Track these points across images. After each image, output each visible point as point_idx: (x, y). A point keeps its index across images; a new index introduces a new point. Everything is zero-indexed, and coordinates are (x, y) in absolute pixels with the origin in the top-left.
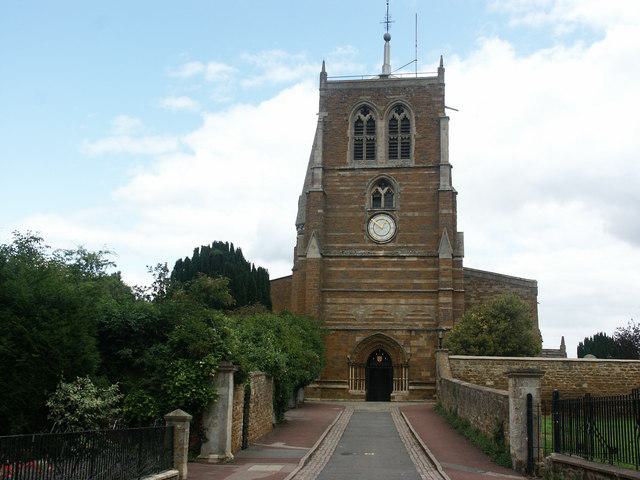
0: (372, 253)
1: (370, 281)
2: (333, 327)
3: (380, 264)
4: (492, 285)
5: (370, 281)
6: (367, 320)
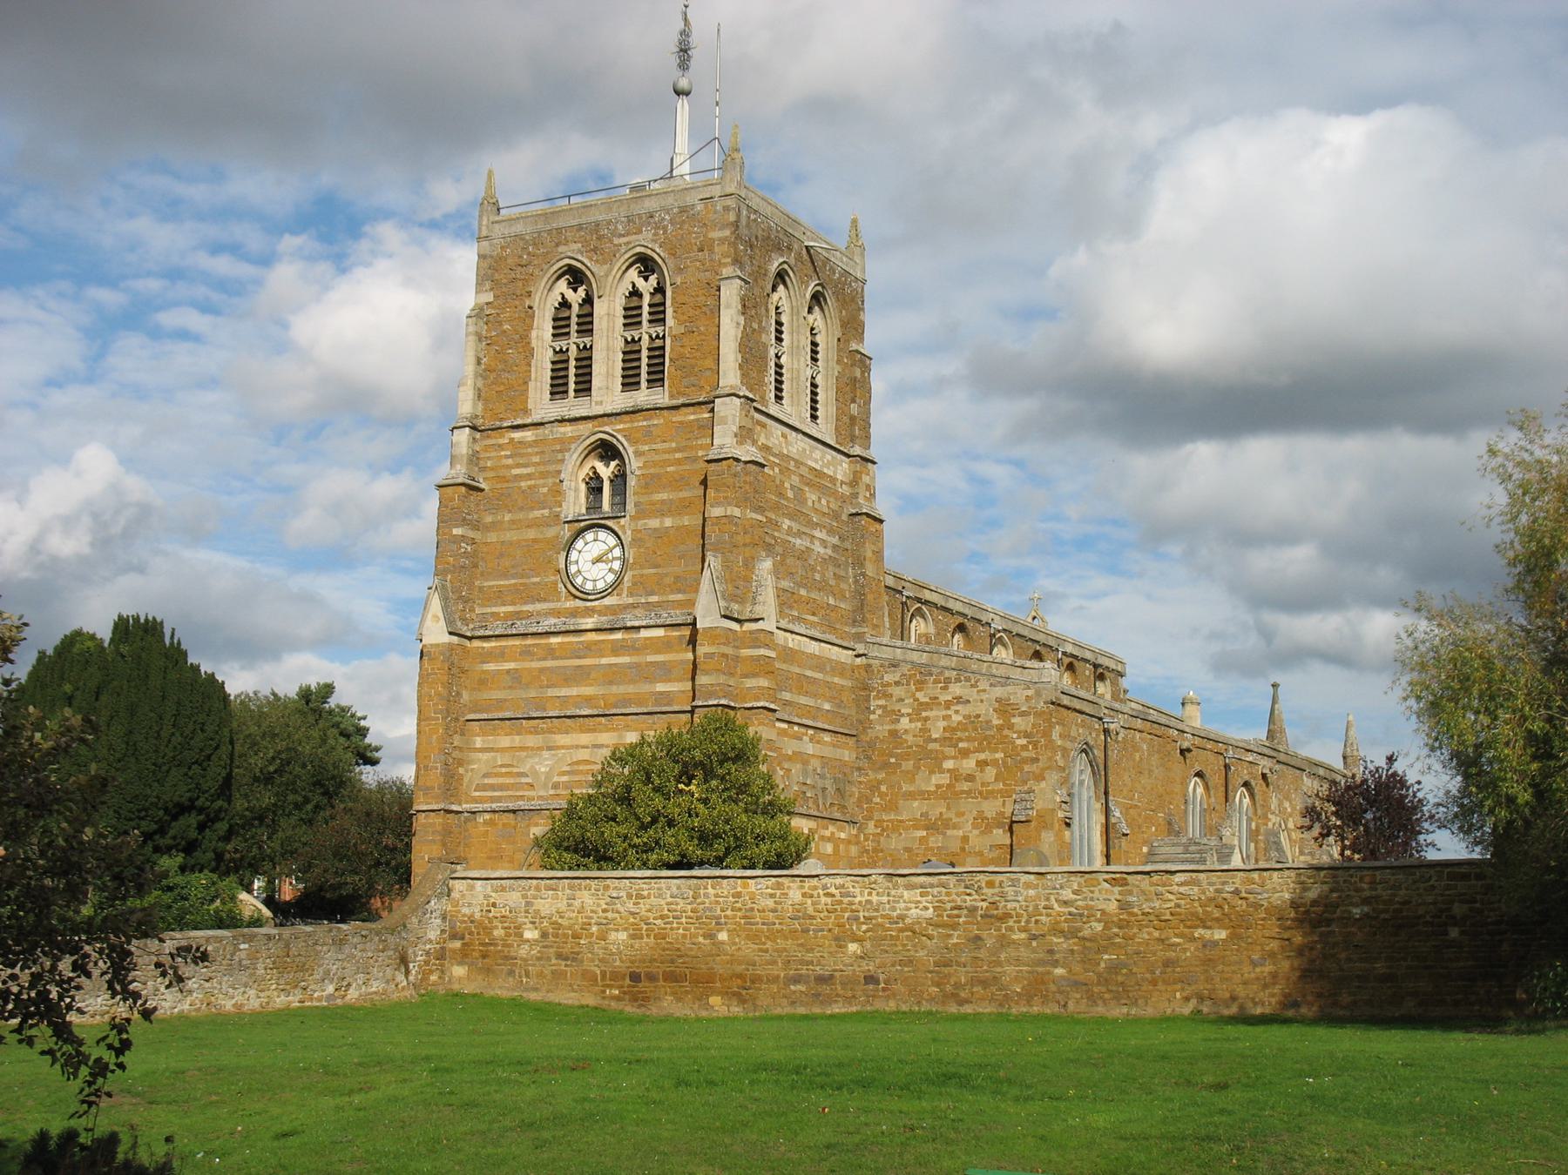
0: (572, 624)
1: (564, 692)
2: (487, 806)
3: (589, 649)
4: (948, 681)
5: (564, 692)
6: (556, 786)
